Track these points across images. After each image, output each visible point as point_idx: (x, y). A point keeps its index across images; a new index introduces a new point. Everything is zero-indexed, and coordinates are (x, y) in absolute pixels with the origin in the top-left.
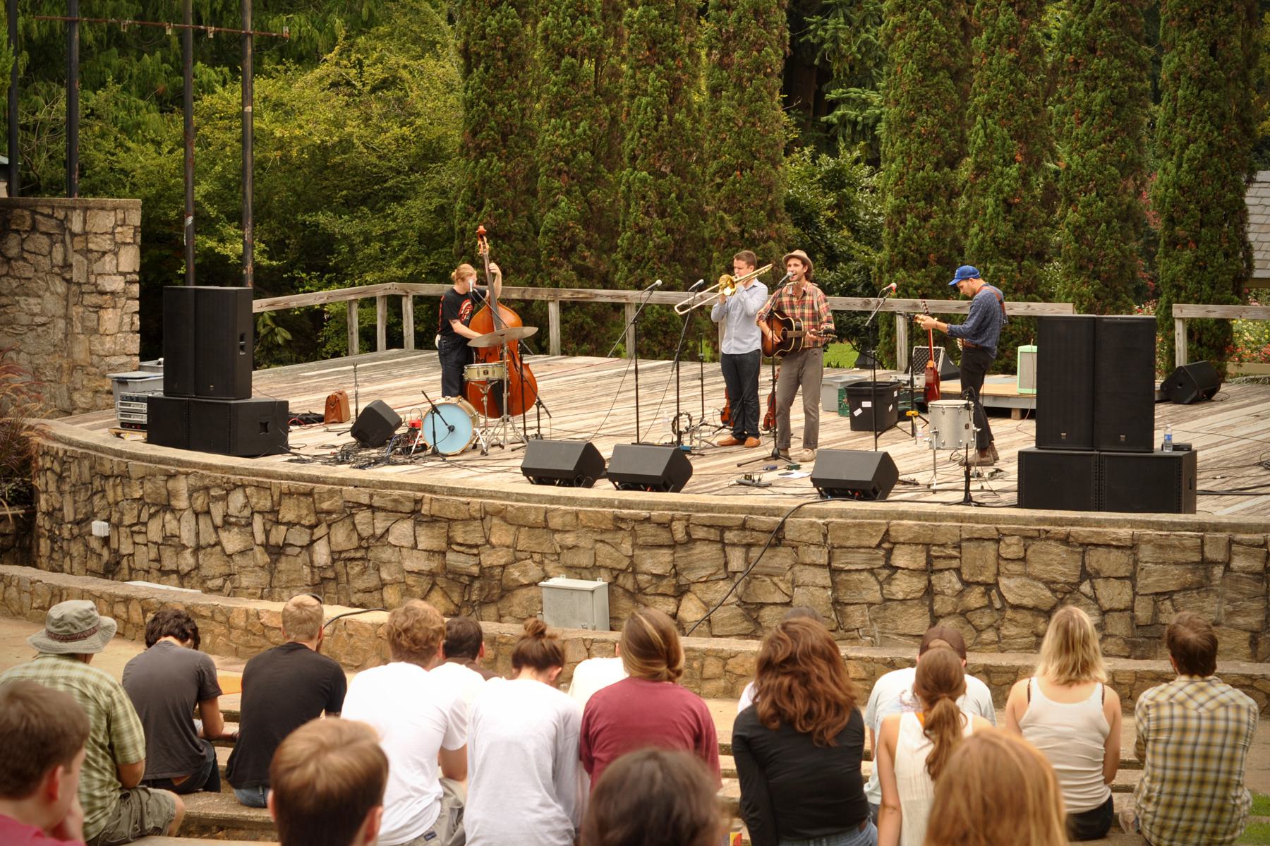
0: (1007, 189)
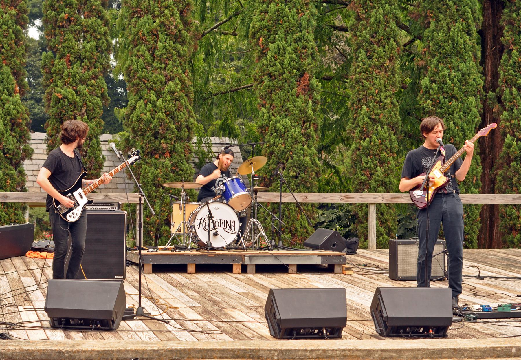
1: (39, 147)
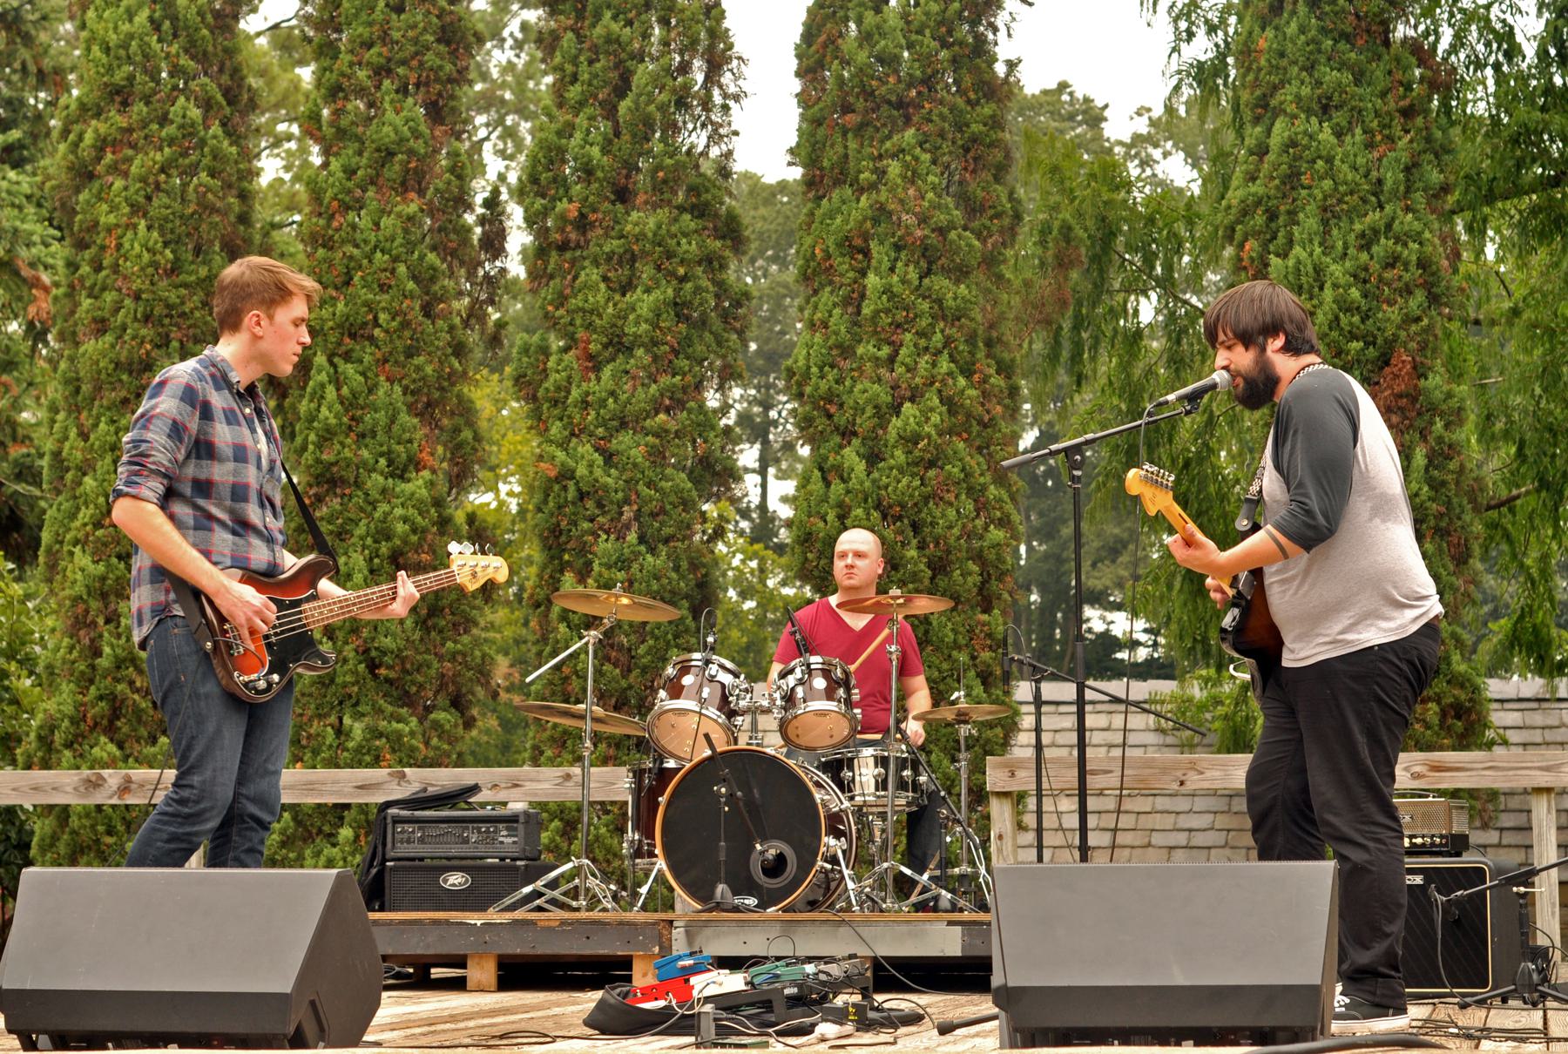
0: (400, 528)
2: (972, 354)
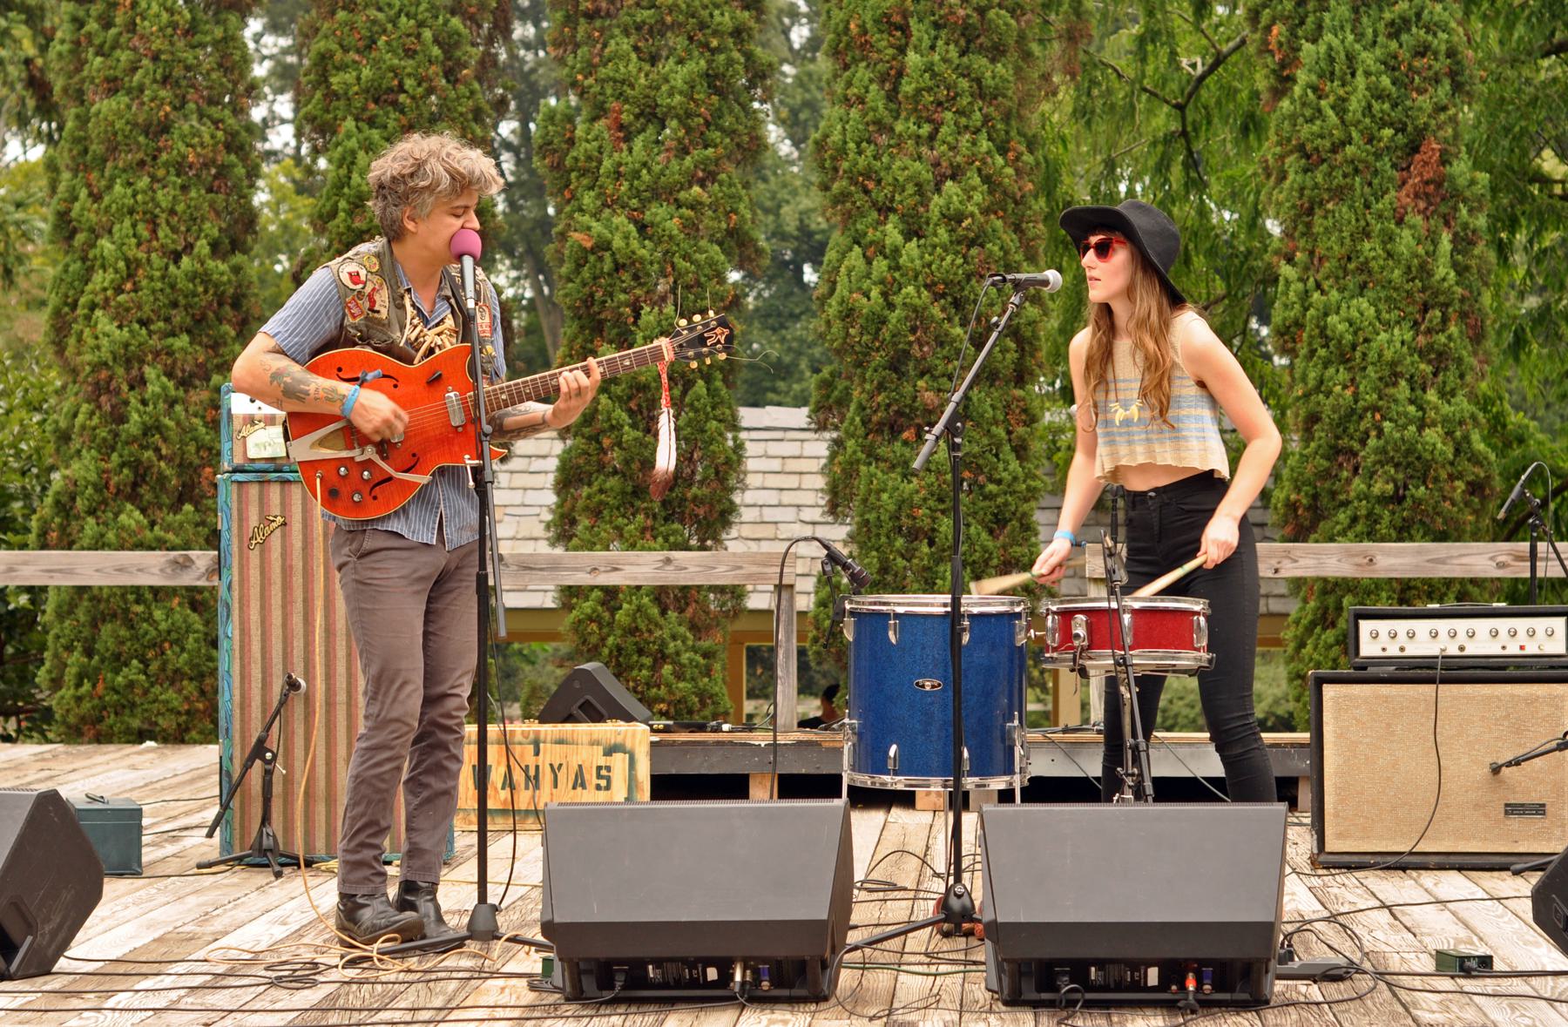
1: (770, 453)
2: (1007, 133)
